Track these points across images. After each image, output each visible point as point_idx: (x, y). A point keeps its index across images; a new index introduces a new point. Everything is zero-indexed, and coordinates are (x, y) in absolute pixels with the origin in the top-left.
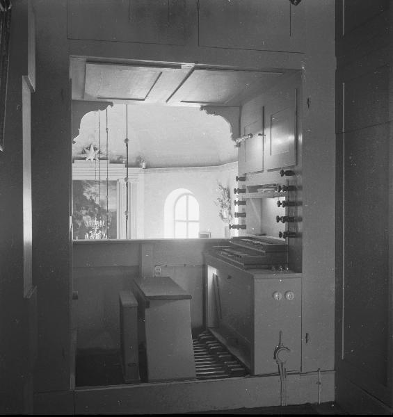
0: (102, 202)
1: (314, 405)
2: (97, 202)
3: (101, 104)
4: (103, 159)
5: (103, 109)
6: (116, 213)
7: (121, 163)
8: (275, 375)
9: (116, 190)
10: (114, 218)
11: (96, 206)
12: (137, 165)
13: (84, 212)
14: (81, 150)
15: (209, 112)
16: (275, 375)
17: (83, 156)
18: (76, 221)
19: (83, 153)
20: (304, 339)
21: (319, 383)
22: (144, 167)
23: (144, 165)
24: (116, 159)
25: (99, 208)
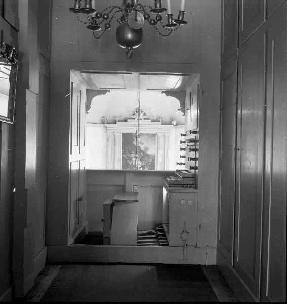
0: (146, 149)
1: (203, 266)
2: (142, 149)
3: (103, 91)
4: (147, 119)
5: (104, 94)
6: (155, 156)
7: (159, 121)
8: (182, 247)
9: (155, 140)
10: (154, 160)
11: (141, 151)
12: (170, 123)
13: (133, 155)
14: (132, 113)
15: (167, 95)
16: (182, 247)
17: (134, 116)
18: (128, 161)
19: (133, 115)
20: (199, 228)
21: (206, 254)
22: (175, 124)
23: (175, 123)
24: (155, 118)
25: (144, 152)
